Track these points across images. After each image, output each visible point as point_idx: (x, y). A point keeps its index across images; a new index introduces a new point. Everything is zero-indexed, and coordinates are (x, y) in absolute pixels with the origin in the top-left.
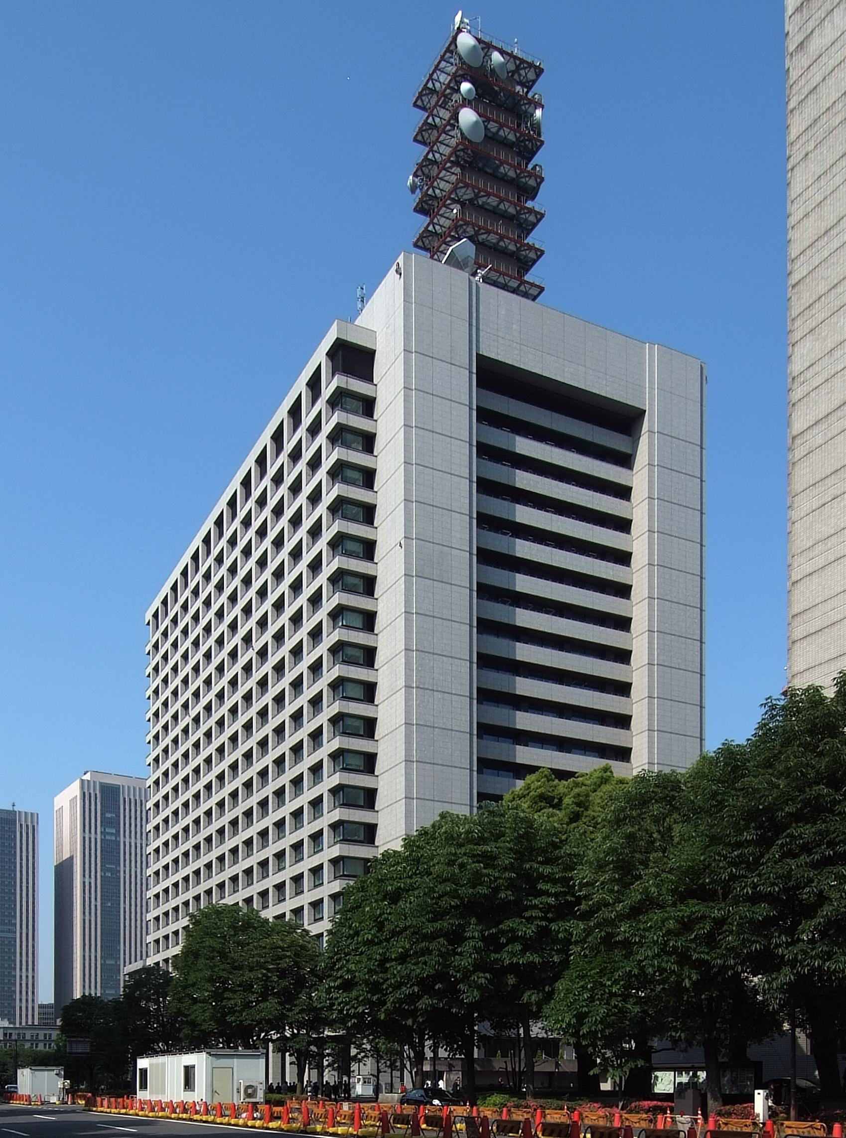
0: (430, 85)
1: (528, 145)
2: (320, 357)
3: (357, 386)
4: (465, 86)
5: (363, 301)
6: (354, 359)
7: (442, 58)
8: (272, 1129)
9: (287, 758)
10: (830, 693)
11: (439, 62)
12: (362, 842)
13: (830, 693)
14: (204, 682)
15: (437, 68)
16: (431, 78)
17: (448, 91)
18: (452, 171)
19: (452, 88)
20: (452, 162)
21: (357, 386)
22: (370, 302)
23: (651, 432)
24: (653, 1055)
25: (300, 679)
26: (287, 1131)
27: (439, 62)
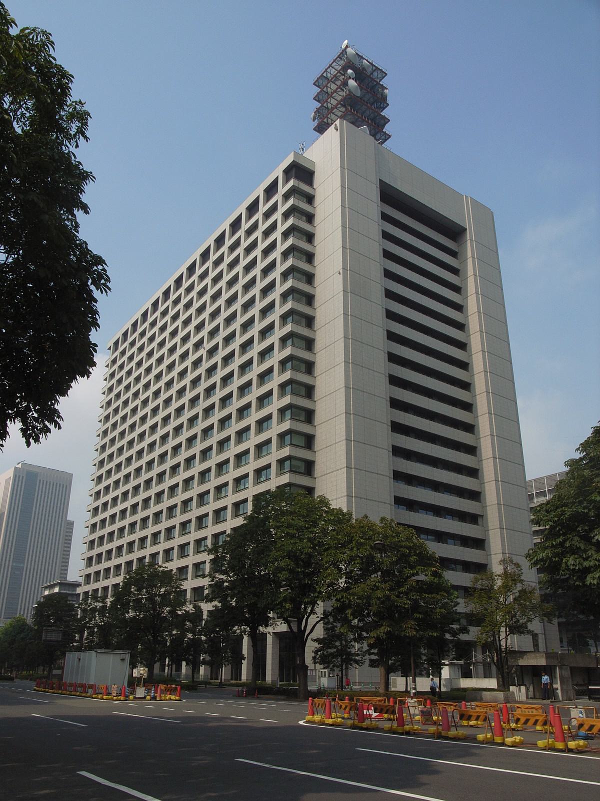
0: (325, 75)
1: (382, 101)
2: (279, 172)
3: (304, 187)
4: (350, 71)
5: (303, 150)
6: (301, 172)
7: (334, 61)
8: (327, 725)
9: (100, 508)
10: (30, 621)
11: (333, 63)
12: (302, 473)
13: (30, 621)
14: (121, 418)
15: (330, 66)
16: (326, 70)
17: (339, 74)
18: (340, 109)
19: (341, 73)
20: (341, 104)
21: (304, 187)
22: (308, 151)
23: (471, 240)
24: (405, 678)
25: (121, 464)
26: (332, 725)
27: (333, 63)
